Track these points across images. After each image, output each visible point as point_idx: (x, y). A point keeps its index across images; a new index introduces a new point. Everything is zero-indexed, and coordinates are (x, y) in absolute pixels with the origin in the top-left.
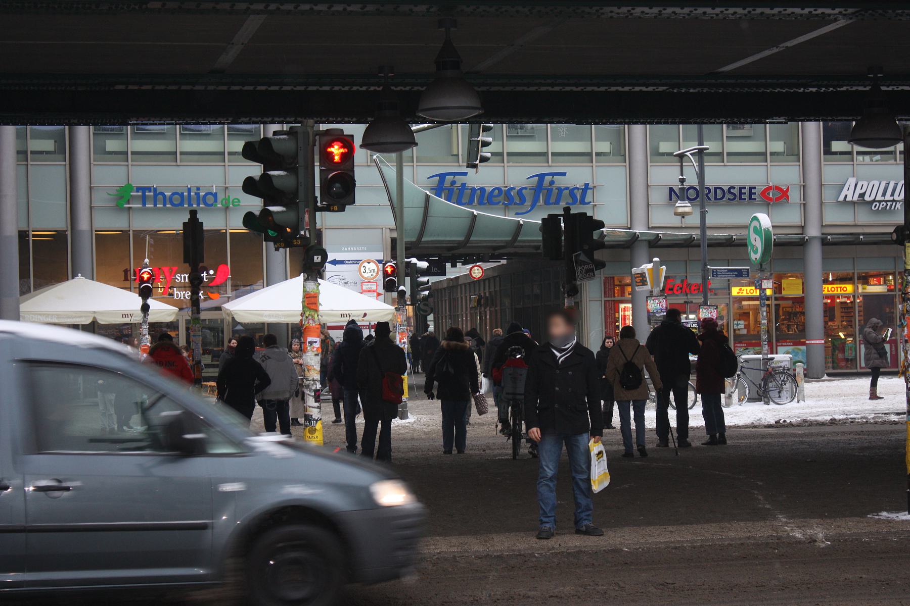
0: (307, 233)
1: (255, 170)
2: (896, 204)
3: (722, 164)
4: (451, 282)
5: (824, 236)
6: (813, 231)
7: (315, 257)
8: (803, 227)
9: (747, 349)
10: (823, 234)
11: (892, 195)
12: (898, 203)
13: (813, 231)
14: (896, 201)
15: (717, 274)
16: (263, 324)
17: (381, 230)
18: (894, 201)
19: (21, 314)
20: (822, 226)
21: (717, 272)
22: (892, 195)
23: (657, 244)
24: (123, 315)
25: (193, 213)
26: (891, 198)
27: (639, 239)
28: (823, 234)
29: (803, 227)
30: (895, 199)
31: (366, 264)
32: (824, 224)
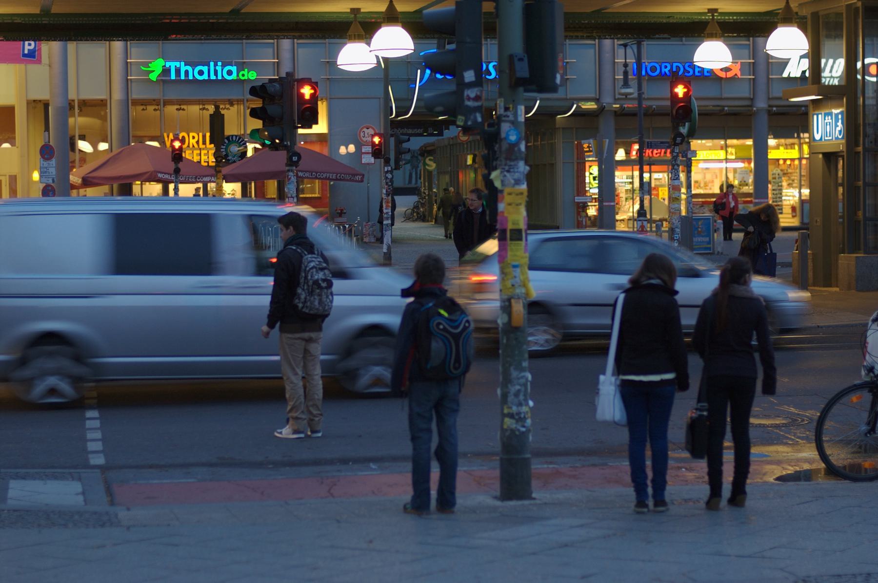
0: (289, 143)
1: (258, 103)
2: (834, 80)
3: (681, 43)
4: (451, 140)
5: (770, 109)
6: (761, 104)
7: (294, 158)
8: (752, 100)
9: (702, 206)
10: (770, 106)
11: (831, 71)
12: (835, 79)
13: (761, 104)
14: (834, 78)
15: (651, 146)
16: (387, 22)
17: (379, 99)
18: (831, 77)
19: (814, 430)
20: (769, 99)
21: (651, 143)
22: (831, 71)
23: (623, 112)
24: (638, 513)
25: (217, 108)
26: (829, 75)
27: (605, 109)
28: (770, 106)
29: (752, 100)
30: (833, 75)
31: (365, 130)
32: (771, 97)
